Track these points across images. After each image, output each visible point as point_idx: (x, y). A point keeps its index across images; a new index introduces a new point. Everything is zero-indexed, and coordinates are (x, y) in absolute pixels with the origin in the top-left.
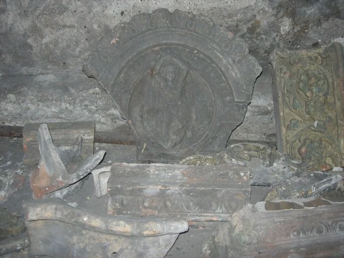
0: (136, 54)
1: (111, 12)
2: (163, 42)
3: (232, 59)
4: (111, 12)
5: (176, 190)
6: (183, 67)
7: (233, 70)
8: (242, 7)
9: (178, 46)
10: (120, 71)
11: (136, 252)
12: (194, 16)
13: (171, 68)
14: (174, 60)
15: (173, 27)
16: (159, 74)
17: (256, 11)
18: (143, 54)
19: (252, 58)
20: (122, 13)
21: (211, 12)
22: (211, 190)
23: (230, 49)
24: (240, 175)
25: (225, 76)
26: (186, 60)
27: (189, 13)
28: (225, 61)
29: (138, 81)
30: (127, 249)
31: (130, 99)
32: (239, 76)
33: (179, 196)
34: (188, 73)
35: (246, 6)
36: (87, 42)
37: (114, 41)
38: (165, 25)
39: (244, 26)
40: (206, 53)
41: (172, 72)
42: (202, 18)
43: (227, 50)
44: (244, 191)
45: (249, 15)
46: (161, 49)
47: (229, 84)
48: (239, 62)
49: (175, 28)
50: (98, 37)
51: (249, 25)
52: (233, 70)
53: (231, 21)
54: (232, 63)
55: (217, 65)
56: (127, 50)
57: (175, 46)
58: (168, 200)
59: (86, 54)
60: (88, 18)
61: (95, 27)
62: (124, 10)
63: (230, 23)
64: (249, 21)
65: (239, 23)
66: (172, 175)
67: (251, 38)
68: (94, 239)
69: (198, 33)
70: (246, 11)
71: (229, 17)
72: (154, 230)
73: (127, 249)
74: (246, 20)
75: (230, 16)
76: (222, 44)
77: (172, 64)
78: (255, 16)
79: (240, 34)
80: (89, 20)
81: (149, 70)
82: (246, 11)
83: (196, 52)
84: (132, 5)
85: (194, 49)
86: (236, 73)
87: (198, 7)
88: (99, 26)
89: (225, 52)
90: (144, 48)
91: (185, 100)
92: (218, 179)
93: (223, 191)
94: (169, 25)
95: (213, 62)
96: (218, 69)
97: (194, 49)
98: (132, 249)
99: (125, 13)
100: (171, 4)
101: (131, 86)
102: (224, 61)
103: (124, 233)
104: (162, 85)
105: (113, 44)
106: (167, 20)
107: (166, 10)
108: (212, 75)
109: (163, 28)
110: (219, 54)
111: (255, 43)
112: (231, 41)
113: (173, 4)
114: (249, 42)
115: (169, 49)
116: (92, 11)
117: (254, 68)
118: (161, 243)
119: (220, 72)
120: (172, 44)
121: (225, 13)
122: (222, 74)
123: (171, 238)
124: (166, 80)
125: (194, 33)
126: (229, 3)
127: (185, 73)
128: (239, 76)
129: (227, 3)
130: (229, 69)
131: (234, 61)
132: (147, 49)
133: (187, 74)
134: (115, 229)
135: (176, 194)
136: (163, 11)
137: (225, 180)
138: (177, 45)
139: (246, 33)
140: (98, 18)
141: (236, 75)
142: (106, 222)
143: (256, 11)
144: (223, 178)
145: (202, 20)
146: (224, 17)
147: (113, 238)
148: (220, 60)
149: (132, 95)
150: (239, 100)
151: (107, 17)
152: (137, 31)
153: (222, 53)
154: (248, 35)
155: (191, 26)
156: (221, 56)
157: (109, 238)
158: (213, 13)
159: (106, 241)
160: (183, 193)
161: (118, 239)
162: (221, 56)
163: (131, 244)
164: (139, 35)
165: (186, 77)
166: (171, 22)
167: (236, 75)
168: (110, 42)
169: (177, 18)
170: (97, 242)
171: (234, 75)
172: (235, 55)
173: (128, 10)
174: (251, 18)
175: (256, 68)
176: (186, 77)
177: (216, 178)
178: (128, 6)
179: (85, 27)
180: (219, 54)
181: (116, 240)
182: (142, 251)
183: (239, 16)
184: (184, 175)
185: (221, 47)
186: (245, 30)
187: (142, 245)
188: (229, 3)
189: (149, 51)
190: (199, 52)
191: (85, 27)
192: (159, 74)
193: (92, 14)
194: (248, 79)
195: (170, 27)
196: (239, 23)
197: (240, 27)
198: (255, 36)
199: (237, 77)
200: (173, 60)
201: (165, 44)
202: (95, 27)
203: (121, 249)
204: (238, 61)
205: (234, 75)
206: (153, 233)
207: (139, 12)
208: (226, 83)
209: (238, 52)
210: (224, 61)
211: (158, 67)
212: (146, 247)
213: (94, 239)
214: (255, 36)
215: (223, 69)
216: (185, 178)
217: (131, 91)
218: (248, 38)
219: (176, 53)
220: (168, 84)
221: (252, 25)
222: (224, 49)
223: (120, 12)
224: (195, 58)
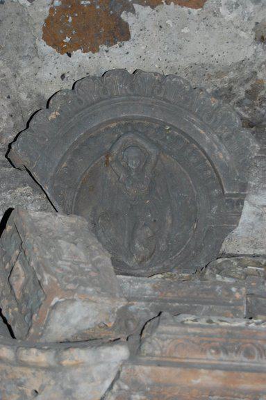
0: (85, 134)
1: (47, 75)
2: (122, 115)
3: (217, 135)
4: (47, 75)
5: (142, 306)
6: (151, 150)
7: (219, 150)
8: (236, 61)
9: (142, 121)
10: (63, 158)
11: (62, 389)
12: (164, 77)
13: (133, 153)
14: (138, 140)
15: (135, 95)
16: (117, 161)
17: (255, 66)
18: (93, 134)
19: (246, 133)
20: (63, 76)
21: (190, 70)
22: (188, 307)
23: (215, 121)
24: (231, 291)
25: (209, 160)
26: (154, 140)
27: (156, 74)
28: (207, 138)
29: (88, 172)
30: (49, 385)
31: (77, 198)
32: (228, 158)
33: (145, 313)
34: (158, 157)
35: (241, 59)
36: (11, 118)
37: (53, 116)
38: (124, 92)
39: (241, 88)
40: (181, 129)
41: (136, 157)
42: (174, 80)
43: (211, 123)
44: (233, 309)
45: (247, 72)
46: (119, 125)
47: (215, 171)
48: (228, 138)
49: (138, 95)
50: (28, 112)
51: (248, 87)
52: (219, 150)
53: (221, 82)
54: (218, 140)
55: (198, 145)
56: (72, 128)
57: (138, 121)
58: (131, 319)
59: (10, 136)
60: (12, 84)
61: (24, 96)
62: (65, 71)
63: (220, 86)
64: (247, 81)
65: (232, 84)
66: (139, 289)
67: (251, 106)
68: (7, 374)
69: (169, 102)
70: (242, 66)
71: (217, 77)
72: (76, 358)
73: (49, 385)
74: (242, 80)
75: (218, 75)
76: (203, 114)
77: (136, 146)
78: (255, 73)
79: (235, 100)
80: (14, 88)
81: (104, 156)
82: (242, 66)
83: (168, 128)
84: (76, 65)
85: (165, 124)
86: (224, 154)
87: (171, 64)
88: (29, 96)
89: (209, 126)
90: (94, 125)
91: (156, 198)
92: (201, 295)
93: (204, 309)
94: (129, 92)
95: (192, 140)
96: (200, 151)
97: (165, 124)
98: (56, 384)
99: (67, 75)
100: (132, 61)
101: (79, 178)
102: (207, 138)
103: (37, 363)
104: (122, 176)
105: (52, 120)
106: (126, 85)
107: (124, 71)
108: (192, 159)
109: (120, 96)
110: (199, 129)
111: (259, 112)
112: (215, 110)
113: (136, 61)
114: (250, 112)
115: (130, 126)
116: (19, 74)
117: (248, 145)
118: (95, 376)
119: (204, 155)
120: (133, 118)
121: (210, 71)
122: (206, 158)
123: (109, 369)
124: (128, 170)
125: (164, 102)
126: (216, 56)
127: (153, 158)
128: (228, 158)
129: (212, 56)
130: (215, 149)
131: (220, 138)
132: (100, 126)
133: (157, 159)
134: (25, 360)
135: (142, 311)
136: (120, 73)
137: (209, 296)
138: (142, 118)
139: (244, 99)
140: (27, 84)
141: (225, 157)
142: (16, 351)
143: (255, 66)
144: (207, 294)
145: (175, 82)
146: (210, 76)
147: (29, 371)
148: (202, 137)
149: (79, 192)
150: (231, 192)
151: (41, 82)
152: (84, 101)
153: (204, 127)
154: (247, 101)
155: (159, 91)
156: (202, 132)
157: (24, 371)
158: (194, 73)
159: (21, 376)
160: (152, 311)
161: (37, 372)
162: (202, 132)
163: (54, 378)
164: (88, 106)
165: (156, 164)
166: (132, 88)
167: (225, 157)
168: (47, 117)
169: (139, 82)
170: (11, 376)
171: (221, 157)
172: (222, 129)
173: (71, 72)
174: (250, 76)
175: (252, 145)
176: (156, 164)
177: (198, 294)
178: (71, 66)
179: (9, 97)
180: (199, 129)
181: (34, 374)
182: (69, 387)
183: (232, 75)
184: (155, 289)
185: (202, 120)
186: (243, 94)
187: (68, 378)
188: (216, 56)
189: (102, 129)
190: (172, 127)
191: (9, 97)
192: (117, 161)
193: (18, 79)
194: (241, 161)
195: (130, 95)
196: (232, 84)
197: (234, 91)
198: (258, 102)
199: (226, 160)
200: (136, 141)
201: (125, 119)
202: (24, 96)
203: (42, 385)
204: (227, 137)
205: (221, 157)
206: (74, 362)
207: (87, 74)
208: (213, 169)
209: (225, 125)
210: (207, 138)
211: (115, 151)
212: (74, 383)
213: (7, 374)
214: (258, 102)
215: (206, 149)
216: (156, 293)
217: (79, 187)
218: (247, 105)
219: (140, 131)
220: (130, 176)
221: (252, 86)
222: (207, 123)
223: (60, 75)
224: (168, 137)
